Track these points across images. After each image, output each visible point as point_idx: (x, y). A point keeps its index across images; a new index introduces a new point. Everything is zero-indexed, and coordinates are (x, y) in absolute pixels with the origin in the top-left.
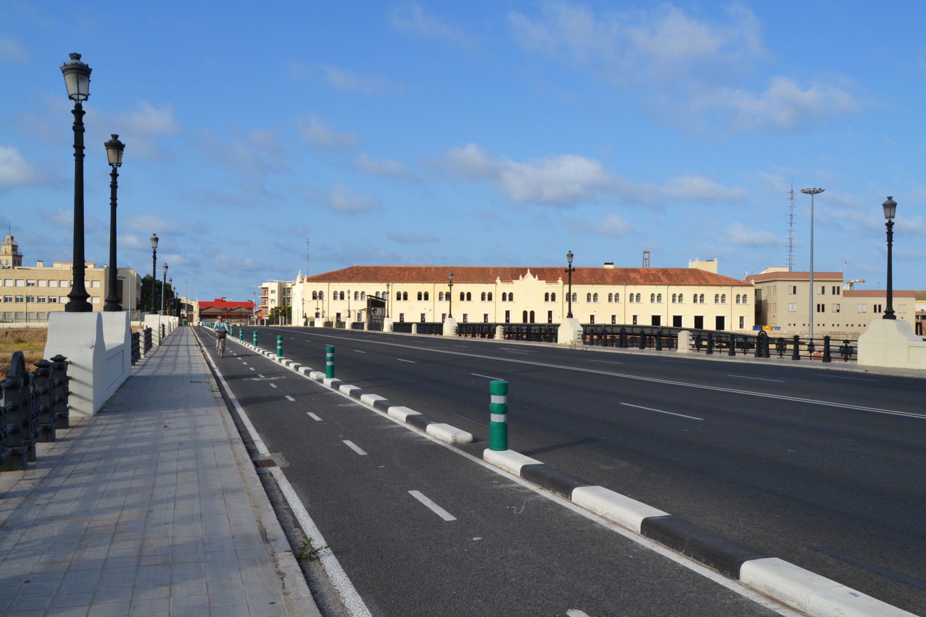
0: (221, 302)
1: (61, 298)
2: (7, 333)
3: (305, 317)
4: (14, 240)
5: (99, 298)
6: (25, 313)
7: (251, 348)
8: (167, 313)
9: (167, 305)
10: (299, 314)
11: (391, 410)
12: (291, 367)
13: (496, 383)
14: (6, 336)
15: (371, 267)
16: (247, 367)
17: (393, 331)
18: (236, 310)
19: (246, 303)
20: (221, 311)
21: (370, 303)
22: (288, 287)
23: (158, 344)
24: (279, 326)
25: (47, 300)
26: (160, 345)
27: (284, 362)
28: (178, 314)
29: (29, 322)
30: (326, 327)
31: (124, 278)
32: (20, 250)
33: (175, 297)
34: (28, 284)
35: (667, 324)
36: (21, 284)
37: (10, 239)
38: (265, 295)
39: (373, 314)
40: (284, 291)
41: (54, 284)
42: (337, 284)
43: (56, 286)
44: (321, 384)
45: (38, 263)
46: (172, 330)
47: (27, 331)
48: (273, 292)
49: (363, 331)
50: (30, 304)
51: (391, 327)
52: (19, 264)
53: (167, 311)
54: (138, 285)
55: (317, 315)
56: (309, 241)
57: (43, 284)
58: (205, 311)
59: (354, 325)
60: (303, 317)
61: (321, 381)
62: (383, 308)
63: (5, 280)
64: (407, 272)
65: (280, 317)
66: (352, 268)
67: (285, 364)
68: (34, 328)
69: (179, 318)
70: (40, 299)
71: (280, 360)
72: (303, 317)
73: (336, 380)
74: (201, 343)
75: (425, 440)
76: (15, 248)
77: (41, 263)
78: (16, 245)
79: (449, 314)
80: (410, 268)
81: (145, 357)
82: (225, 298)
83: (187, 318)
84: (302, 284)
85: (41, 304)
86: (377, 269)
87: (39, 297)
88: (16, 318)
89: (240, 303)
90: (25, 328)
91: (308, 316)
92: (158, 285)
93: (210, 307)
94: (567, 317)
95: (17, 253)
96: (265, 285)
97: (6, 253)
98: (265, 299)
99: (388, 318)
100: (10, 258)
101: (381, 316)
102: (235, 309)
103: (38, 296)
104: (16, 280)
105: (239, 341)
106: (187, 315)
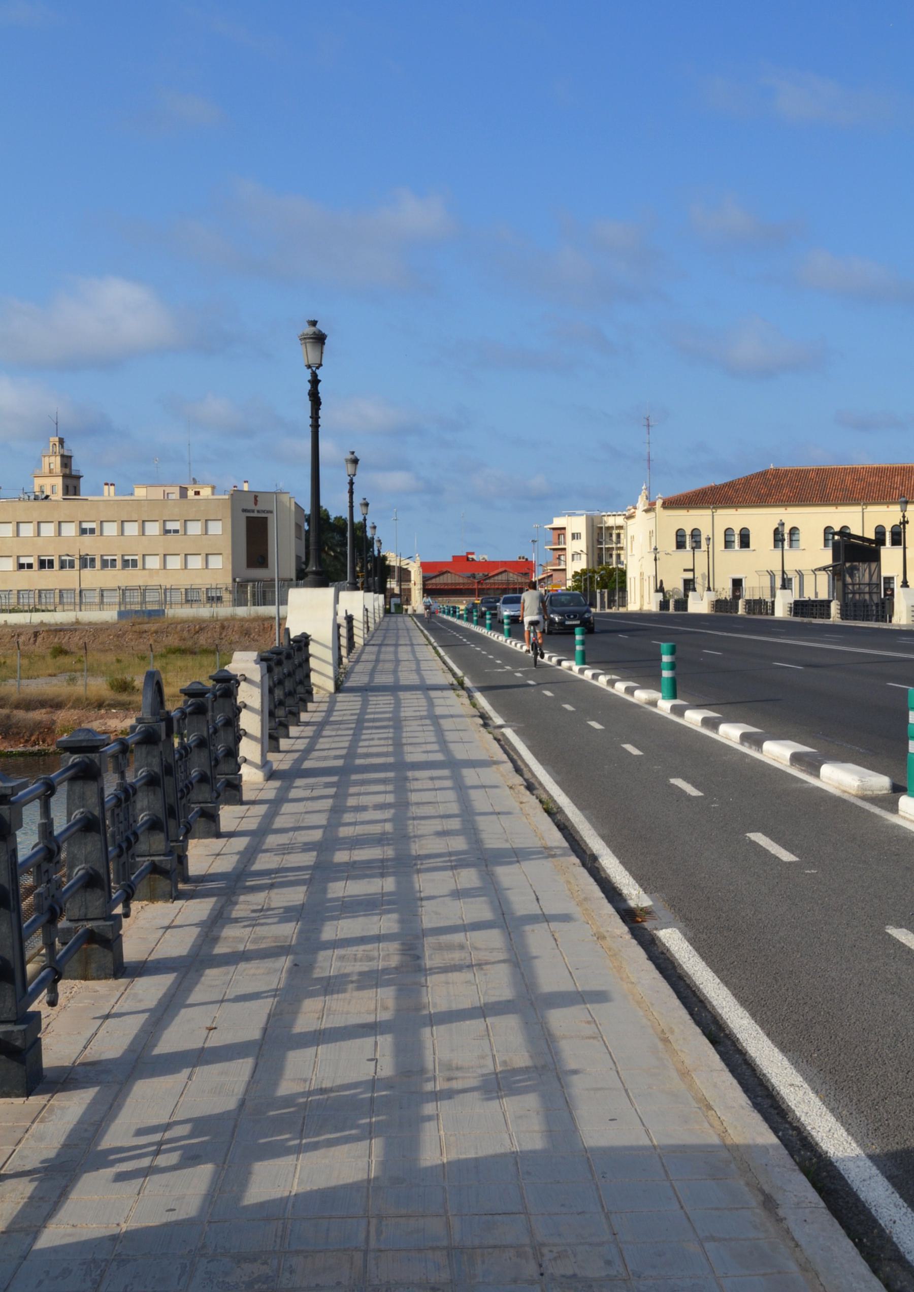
0: (464, 560)
1: (147, 558)
2: (36, 634)
3: (660, 589)
4: (65, 445)
5: (220, 557)
6: (77, 592)
7: (570, 669)
8: (359, 585)
9: (358, 569)
10: (646, 584)
11: (768, 746)
12: (603, 680)
13: (665, 647)
14: (35, 641)
15: (808, 471)
16: (511, 673)
17: (794, 616)
18: (496, 578)
19: (517, 562)
20: (466, 581)
21: (842, 551)
22: (606, 525)
23: (330, 686)
24: (598, 610)
25: (119, 564)
26: (339, 688)
27: (588, 674)
28: (381, 589)
29: (81, 610)
30: (718, 614)
31: (271, 512)
32: (77, 466)
33: (376, 553)
34: (83, 531)
35: (816, 594)
36: (70, 530)
37: (57, 444)
38: (559, 544)
39: (848, 580)
40: (600, 534)
41: (132, 529)
42: (731, 511)
43: (137, 534)
44: (654, 710)
45: (106, 487)
46: (372, 626)
47: (76, 630)
48: (575, 536)
49: (831, 621)
50: (87, 572)
51: (791, 608)
52: (76, 491)
53: (360, 581)
54: (298, 527)
55: (689, 585)
56: (651, 424)
57: (111, 529)
58: (433, 581)
59: (800, 607)
60: (657, 591)
61: (654, 704)
62: (874, 565)
63: (39, 523)
64: (898, 479)
65: (598, 591)
66: (764, 474)
67: (606, 684)
68: (90, 624)
69: (385, 597)
70: (128, 560)
71: (581, 671)
72: (657, 591)
73: (678, 702)
74: (492, 713)
75: (806, 785)
76: (66, 461)
77: (112, 488)
78: (69, 454)
79: (901, 578)
80: (903, 469)
81: (350, 662)
82: (473, 554)
83: (399, 596)
84: (652, 514)
85: (109, 572)
86: (824, 475)
87: (105, 558)
88: (61, 603)
89: (505, 563)
90: (73, 624)
91: (667, 587)
92: (339, 527)
93: (442, 573)
94: (902, 586)
95: (71, 469)
96: (558, 522)
97: (51, 471)
98: (560, 553)
99: (709, 592)
100: (59, 482)
101: (869, 584)
102: (493, 576)
103: (102, 556)
104: (60, 522)
105: (504, 639)
106: (401, 589)
